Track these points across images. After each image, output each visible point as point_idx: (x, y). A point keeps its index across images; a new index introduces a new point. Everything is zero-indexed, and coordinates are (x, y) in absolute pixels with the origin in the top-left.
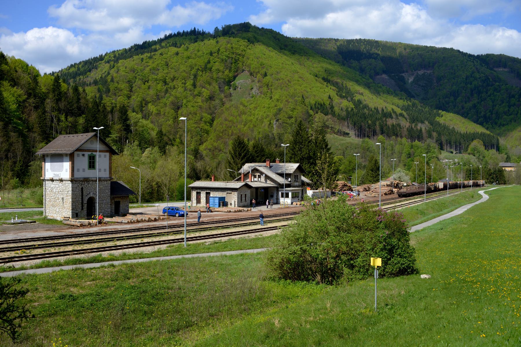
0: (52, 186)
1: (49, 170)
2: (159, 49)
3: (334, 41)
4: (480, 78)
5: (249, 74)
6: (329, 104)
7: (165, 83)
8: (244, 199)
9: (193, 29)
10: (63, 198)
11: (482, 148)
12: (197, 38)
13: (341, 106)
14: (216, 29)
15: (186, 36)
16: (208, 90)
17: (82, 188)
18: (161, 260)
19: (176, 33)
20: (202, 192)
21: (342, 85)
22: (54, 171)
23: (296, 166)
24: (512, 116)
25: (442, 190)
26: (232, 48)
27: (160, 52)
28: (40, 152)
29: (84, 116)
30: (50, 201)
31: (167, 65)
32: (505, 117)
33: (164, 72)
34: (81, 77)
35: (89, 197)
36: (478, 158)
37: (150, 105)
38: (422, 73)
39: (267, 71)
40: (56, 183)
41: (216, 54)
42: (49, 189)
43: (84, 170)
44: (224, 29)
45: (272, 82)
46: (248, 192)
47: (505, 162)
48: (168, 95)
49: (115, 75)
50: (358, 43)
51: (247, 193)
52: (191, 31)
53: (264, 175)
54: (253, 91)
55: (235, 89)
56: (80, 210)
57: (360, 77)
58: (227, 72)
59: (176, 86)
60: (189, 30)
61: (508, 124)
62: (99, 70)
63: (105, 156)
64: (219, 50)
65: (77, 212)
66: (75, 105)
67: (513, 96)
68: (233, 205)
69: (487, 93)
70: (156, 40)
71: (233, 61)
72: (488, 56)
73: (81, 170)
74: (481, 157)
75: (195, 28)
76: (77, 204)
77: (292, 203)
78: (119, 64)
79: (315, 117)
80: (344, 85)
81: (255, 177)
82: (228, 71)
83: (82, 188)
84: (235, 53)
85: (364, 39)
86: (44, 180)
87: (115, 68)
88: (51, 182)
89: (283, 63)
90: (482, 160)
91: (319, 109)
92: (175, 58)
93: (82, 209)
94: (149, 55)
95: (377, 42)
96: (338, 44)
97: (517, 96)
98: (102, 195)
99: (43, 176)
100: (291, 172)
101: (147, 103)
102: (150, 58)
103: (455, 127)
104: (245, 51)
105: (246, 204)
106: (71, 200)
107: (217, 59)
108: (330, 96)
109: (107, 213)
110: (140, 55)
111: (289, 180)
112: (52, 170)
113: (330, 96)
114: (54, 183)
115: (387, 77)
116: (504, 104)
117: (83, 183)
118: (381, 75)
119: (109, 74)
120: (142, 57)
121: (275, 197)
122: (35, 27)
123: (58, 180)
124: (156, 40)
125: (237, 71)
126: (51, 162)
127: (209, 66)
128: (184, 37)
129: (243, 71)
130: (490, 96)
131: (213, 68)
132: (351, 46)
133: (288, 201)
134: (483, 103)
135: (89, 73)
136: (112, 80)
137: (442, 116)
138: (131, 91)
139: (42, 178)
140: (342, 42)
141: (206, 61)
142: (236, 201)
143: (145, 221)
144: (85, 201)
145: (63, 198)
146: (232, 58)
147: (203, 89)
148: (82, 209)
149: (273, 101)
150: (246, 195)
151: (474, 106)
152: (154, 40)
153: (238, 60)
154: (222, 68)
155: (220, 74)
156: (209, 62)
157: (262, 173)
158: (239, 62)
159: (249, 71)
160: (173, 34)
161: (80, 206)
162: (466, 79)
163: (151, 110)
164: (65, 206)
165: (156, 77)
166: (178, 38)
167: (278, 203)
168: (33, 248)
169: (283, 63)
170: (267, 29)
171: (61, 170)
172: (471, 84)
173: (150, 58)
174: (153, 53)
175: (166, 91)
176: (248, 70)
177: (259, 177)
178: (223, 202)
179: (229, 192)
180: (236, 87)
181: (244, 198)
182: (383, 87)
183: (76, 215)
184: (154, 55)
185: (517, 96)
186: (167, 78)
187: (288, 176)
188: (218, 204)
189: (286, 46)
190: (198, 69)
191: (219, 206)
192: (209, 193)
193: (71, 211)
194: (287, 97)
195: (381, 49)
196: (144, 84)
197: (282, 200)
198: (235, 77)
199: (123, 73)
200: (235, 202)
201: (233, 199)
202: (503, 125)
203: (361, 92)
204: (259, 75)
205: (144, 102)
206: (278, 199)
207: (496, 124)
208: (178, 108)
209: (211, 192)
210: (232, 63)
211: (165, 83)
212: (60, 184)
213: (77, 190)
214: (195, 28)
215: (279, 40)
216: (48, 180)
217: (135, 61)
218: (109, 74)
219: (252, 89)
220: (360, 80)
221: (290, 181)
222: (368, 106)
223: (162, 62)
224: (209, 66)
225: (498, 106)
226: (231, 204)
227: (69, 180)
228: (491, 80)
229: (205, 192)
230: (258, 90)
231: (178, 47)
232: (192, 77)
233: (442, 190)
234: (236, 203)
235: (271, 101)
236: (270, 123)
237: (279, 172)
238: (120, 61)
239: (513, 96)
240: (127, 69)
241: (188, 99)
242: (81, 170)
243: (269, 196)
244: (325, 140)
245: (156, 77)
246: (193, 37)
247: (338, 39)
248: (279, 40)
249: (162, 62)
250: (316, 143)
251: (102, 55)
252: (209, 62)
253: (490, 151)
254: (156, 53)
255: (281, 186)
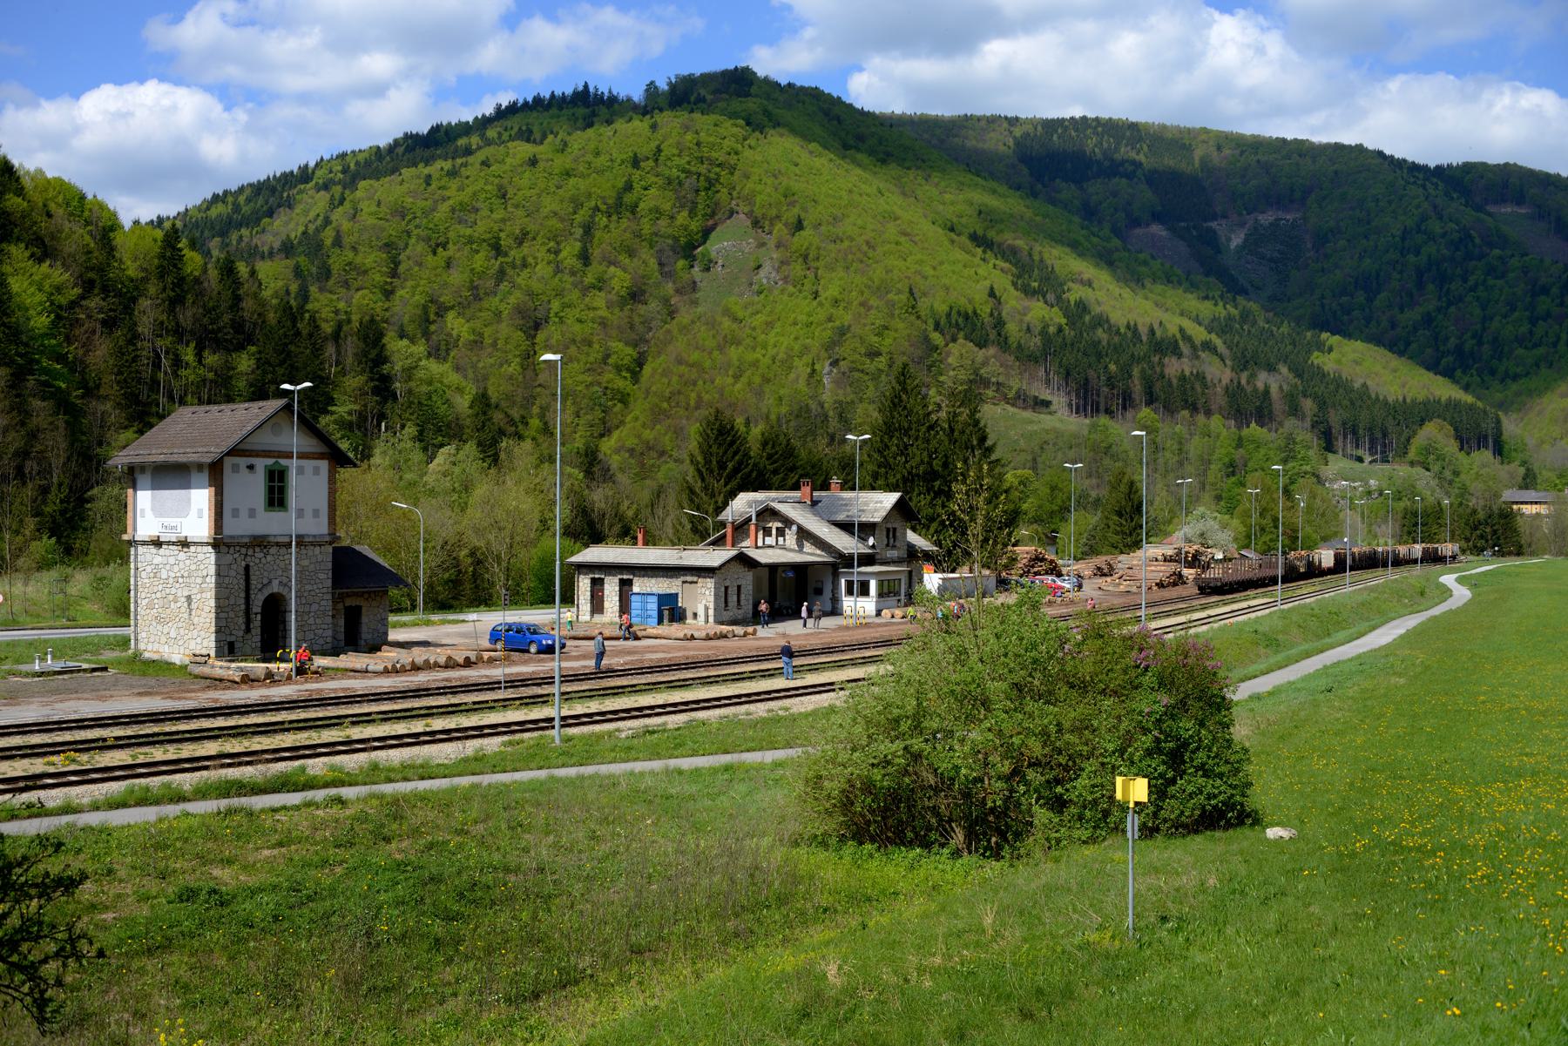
0: (157, 560)
1: (149, 513)
2: (479, 148)
3: (1005, 125)
4: (1444, 235)
5: (749, 223)
6: (991, 314)
7: (497, 249)
8: (733, 599)
9: (581, 88)
10: (189, 598)
11: (1451, 447)
12: (594, 114)
13: (1028, 318)
14: (651, 89)
15: (561, 109)
16: (625, 270)
17: (247, 568)
18: (485, 783)
19: (530, 99)
20: (608, 580)
21: (1030, 255)
22: (161, 516)
23: (890, 499)
24: (1541, 351)
25: (1330, 571)
26: (698, 144)
27: (480, 156)
28: (119, 459)
29: (253, 349)
30: (150, 606)
31: (504, 196)
32: (1520, 351)
33: (495, 216)
34: (245, 232)
35: (267, 592)
36: (1439, 476)
37: (451, 315)
38: (1271, 219)
39: (803, 215)
40: (167, 552)
41: (651, 163)
42: (149, 569)
43: (252, 513)
44: (673, 87)
45: (819, 248)
46: (747, 579)
47: (1521, 488)
48: (504, 286)
49: (346, 226)
50: (1077, 130)
51: (742, 582)
52: (576, 94)
53: (794, 528)
54: (762, 273)
55: (708, 269)
56: (241, 633)
57: (1084, 232)
58: (683, 217)
59: (530, 260)
60: (569, 91)
61: (1527, 374)
62: (297, 211)
63: (316, 471)
64: (659, 150)
65: (233, 639)
66: (226, 318)
67: (1545, 290)
68: (701, 618)
69: (1465, 281)
70: (471, 120)
71: (703, 183)
72: (1468, 168)
73: (244, 513)
74: (1448, 474)
75: (586, 86)
76: (232, 614)
77: (879, 613)
78: (359, 194)
79: (948, 354)
80: (1036, 258)
81: (767, 532)
82: (685, 213)
83: (247, 568)
84: (708, 159)
85: (1097, 119)
86: (132, 543)
87: (347, 204)
88: (153, 549)
89: (850, 191)
90: (1451, 483)
91: (960, 329)
92: (527, 175)
93: (248, 630)
94: (447, 165)
95: (1134, 126)
96: (1018, 132)
97: (1555, 290)
98: (308, 587)
99: (129, 530)
100: (877, 518)
101: (442, 311)
102: (453, 173)
103: (1369, 383)
104: (736, 153)
105: (739, 614)
106: (212, 603)
107: (654, 179)
108: (992, 288)
109: (321, 641)
110: (421, 165)
111: (871, 541)
112: (158, 511)
113: (992, 288)
114: (162, 551)
115: (1164, 233)
116: (1517, 314)
117: (250, 552)
118: (1148, 225)
119: (327, 222)
120: (426, 171)
121: (827, 594)
122: (106, 81)
123: (173, 543)
124: (471, 120)
125: (713, 214)
126: (153, 488)
127: (628, 199)
128: (554, 111)
129: (732, 213)
130: (1473, 289)
131: (642, 205)
132: (1055, 137)
133: (868, 605)
134: (1452, 309)
135: (267, 220)
136: (338, 242)
137: (1330, 350)
138: (394, 274)
139: (125, 537)
140: (1029, 128)
141: (620, 184)
142: (712, 606)
143: (436, 665)
144: (257, 607)
145: (189, 598)
146: (699, 175)
147: (612, 269)
148: (248, 630)
149: (821, 304)
150: (739, 587)
151: (1428, 320)
152: (464, 120)
153: (717, 180)
154: (667, 206)
155: (663, 223)
156: (629, 187)
157: (788, 522)
158: (718, 187)
159: (749, 214)
160: (521, 101)
161: (241, 620)
162: (1403, 239)
163: (455, 333)
164: (196, 620)
165: (468, 231)
166: (535, 114)
167: (835, 611)
168: (101, 748)
169: (850, 191)
170: (802, 88)
171: (183, 511)
172: (1418, 253)
173: (453, 173)
174: (459, 161)
175: (501, 275)
176: (746, 210)
177: (780, 532)
178: (671, 610)
179: (689, 578)
180: (710, 261)
181: (735, 598)
182: (1152, 262)
183: (228, 648)
184: (465, 165)
185: (1555, 290)
186: (502, 235)
187: (866, 529)
188: (655, 614)
189: (861, 138)
190: (597, 209)
191: (660, 622)
192: (629, 583)
193: (213, 637)
194: (862, 293)
195: (1145, 148)
196: (435, 253)
197: (848, 603)
198: (706, 233)
199: (371, 221)
200: (707, 609)
201: (701, 599)
202: (1515, 378)
203: (1086, 277)
204: (779, 226)
205: (433, 309)
206: (836, 600)
207: (1493, 373)
208: (537, 326)
209: (636, 580)
210: (697, 191)
211: (497, 249)
212: (182, 556)
213: (233, 573)
214: (586, 86)
215: (839, 121)
216: (144, 543)
217: (406, 185)
218: (327, 222)
219: (759, 267)
220: (1082, 240)
221: (873, 547)
222: (1108, 321)
223: (489, 187)
224: (628, 199)
225: (1498, 318)
226: (695, 615)
227: (208, 544)
228: (1477, 241)
229: (616, 580)
230: (778, 270)
231: (534, 142)
232: (579, 232)
233: (1330, 571)
234: (711, 612)
235: (815, 303)
236: (814, 371)
237: (841, 517)
238: (363, 184)
239: (1545, 290)
240: (383, 209)
241: (566, 300)
242: (244, 513)
243: (810, 591)
244: (977, 422)
245: (468, 231)
246: (581, 111)
247: (1017, 119)
248: (839, 121)
249: (489, 187)
250: (952, 430)
251: (306, 166)
252: (629, 187)
253: (1475, 455)
254: (471, 159)
255: (847, 561)
